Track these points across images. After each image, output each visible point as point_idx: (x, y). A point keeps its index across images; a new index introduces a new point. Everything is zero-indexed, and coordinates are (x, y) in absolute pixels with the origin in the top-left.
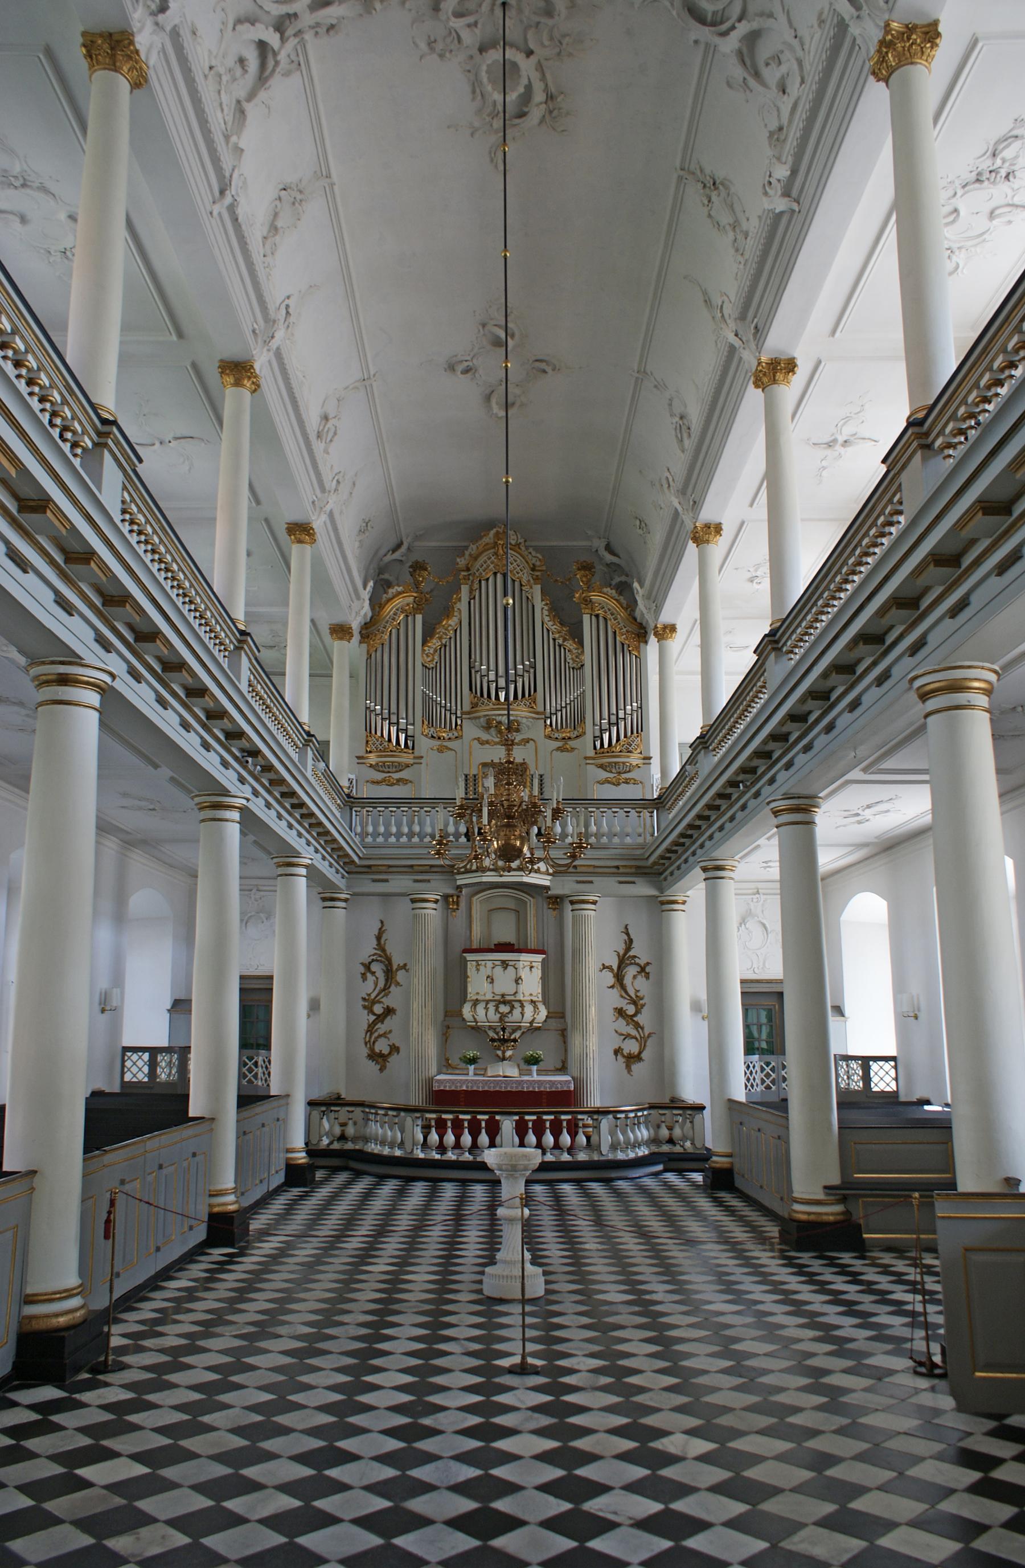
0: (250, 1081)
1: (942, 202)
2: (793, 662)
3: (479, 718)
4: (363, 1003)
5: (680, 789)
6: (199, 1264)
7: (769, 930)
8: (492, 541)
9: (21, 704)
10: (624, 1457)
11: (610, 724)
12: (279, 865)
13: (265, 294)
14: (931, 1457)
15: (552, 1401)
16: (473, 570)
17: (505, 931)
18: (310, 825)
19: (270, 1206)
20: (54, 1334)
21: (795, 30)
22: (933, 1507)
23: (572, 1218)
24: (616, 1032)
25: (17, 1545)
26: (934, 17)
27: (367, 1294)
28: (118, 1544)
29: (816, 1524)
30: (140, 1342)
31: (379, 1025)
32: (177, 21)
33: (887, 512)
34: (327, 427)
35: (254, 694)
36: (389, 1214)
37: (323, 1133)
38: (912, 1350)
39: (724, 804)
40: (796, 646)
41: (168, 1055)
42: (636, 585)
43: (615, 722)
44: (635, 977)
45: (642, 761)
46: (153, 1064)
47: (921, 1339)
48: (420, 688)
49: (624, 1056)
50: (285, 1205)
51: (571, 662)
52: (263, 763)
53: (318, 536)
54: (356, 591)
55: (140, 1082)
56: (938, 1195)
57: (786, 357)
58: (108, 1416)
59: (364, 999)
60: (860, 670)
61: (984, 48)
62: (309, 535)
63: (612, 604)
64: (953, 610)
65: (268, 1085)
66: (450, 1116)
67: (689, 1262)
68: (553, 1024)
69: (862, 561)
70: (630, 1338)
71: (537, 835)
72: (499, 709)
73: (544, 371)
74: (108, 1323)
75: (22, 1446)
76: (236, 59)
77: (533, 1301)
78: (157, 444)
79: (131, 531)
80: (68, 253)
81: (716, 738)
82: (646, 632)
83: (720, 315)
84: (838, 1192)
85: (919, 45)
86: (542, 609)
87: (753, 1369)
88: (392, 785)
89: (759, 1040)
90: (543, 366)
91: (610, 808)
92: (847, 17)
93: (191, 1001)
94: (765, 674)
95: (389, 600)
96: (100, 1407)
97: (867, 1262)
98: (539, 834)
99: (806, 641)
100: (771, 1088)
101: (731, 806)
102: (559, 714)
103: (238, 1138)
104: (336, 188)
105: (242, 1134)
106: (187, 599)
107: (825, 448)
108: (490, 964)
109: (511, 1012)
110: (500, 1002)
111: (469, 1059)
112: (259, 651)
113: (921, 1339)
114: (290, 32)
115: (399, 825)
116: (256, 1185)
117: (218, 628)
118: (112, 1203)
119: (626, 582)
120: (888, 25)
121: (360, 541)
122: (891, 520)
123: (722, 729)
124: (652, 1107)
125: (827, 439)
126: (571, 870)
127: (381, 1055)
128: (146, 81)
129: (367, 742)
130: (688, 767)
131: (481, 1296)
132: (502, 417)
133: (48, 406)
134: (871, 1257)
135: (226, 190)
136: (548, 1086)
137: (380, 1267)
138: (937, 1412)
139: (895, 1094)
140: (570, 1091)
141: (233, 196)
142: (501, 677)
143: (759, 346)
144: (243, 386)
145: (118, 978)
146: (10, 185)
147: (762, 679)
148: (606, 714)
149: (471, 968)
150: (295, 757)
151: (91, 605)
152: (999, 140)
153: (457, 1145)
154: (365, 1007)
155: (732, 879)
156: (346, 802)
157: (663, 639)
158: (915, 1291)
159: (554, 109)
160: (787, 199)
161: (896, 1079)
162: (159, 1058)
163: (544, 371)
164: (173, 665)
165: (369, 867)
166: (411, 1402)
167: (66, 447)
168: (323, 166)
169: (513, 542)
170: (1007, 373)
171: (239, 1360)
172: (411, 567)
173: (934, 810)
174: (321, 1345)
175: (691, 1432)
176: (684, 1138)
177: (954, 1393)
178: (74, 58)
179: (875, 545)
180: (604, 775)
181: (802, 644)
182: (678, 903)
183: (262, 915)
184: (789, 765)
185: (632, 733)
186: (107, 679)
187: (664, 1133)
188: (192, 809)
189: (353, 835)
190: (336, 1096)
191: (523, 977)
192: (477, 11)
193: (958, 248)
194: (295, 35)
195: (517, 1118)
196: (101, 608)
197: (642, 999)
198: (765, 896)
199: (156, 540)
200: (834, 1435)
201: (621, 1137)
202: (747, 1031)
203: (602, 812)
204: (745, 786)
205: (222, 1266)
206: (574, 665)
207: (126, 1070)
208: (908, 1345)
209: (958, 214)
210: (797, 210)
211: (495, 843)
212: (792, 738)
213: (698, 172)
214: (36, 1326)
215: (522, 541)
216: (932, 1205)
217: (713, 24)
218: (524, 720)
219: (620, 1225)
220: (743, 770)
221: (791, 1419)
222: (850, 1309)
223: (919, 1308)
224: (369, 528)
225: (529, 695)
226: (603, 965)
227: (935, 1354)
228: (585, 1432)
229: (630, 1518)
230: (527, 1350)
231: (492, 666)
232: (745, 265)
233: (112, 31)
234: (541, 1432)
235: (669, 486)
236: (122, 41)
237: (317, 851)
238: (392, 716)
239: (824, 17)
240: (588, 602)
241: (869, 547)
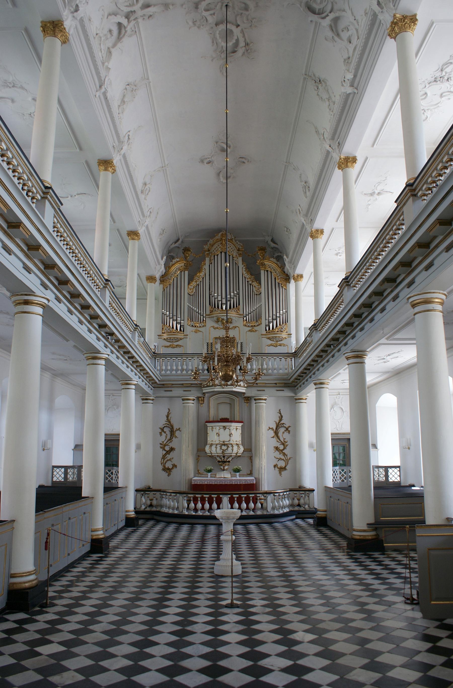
0: (109, 481)
1: (420, 90)
2: (355, 291)
3: (214, 317)
4: (160, 446)
5: (305, 348)
6: (87, 561)
7: (344, 411)
8: (220, 238)
9: (8, 313)
10: (276, 642)
11: (273, 319)
12: (123, 384)
13: (119, 130)
14: (411, 638)
15: (245, 619)
16: (211, 251)
17: (225, 413)
18: (137, 366)
19: (118, 536)
20: (24, 591)
21: (355, 17)
22: (411, 659)
23: (254, 540)
24: (275, 457)
25: (11, 679)
26: (415, 13)
27: (162, 574)
28: (55, 679)
29: (360, 668)
30: (61, 595)
31: (167, 455)
32: (82, 15)
33: (397, 224)
34: (146, 187)
35: (112, 308)
36: (172, 539)
37: (142, 503)
38: (404, 593)
39: (324, 355)
40: (357, 284)
41: (73, 469)
42: (285, 257)
43: (275, 318)
44: (283, 433)
45: (288, 336)
46: (66, 473)
47: (409, 588)
48: (187, 304)
49: (278, 468)
50: (125, 535)
51: (255, 291)
52: (115, 338)
53: (141, 237)
54: (158, 261)
55: (60, 481)
56: (417, 526)
57: (352, 156)
58: (48, 626)
59: (161, 444)
60: (385, 294)
61: (436, 26)
62: (137, 236)
63: (274, 265)
64: (427, 267)
65: (118, 483)
66: (200, 496)
67: (307, 558)
68: (246, 454)
69: (386, 246)
70: (280, 591)
71: (239, 370)
72: (223, 313)
73: (244, 162)
74: (47, 586)
75: (11, 638)
76: (108, 30)
77: (236, 576)
78: (70, 197)
79: (57, 236)
80: (32, 115)
81: (321, 325)
82: (289, 278)
83: (323, 138)
84: (373, 526)
85: (409, 24)
86: (243, 268)
87: (334, 603)
88: (174, 348)
89: (339, 460)
90: (243, 160)
91: (273, 357)
92: (377, 12)
93: (83, 445)
94: (343, 296)
95: (173, 265)
96: (44, 622)
97: (385, 556)
98: (241, 369)
99: (361, 281)
100: (344, 481)
101: (327, 355)
102: (250, 315)
103: (104, 506)
104: (151, 84)
105: (106, 504)
106: (82, 266)
107: (370, 196)
108: (218, 428)
109: (227, 449)
110: (222, 445)
111: (208, 470)
112: (114, 288)
113: (409, 588)
114: (132, 18)
115: (177, 366)
116: (112, 526)
117: (96, 278)
118: (48, 534)
119: (280, 256)
120: (395, 15)
121: (160, 239)
122: (399, 227)
123: (323, 321)
124: (291, 490)
125: (370, 192)
126: (255, 385)
127: (168, 469)
128: (68, 40)
129: (163, 328)
130: (308, 338)
131: (213, 574)
132: (224, 183)
133: (21, 181)
134: (387, 554)
135: (102, 86)
136: (244, 481)
137: (168, 562)
138: (414, 619)
139: (399, 483)
140: (254, 484)
141: (105, 88)
142: (224, 298)
143: (340, 151)
144: (108, 170)
145: (50, 435)
146: (8, 86)
147: (342, 299)
148: (271, 315)
149: (209, 429)
150: (130, 336)
151: (39, 269)
152: (444, 64)
153: (203, 508)
154: (161, 448)
155: (327, 388)
156: (153, 355)
157: (297, 281)
158: (406, 568)
159: (249, 49)
160: (352, 88)
161: (400, 476)
162: (69, 471)
163: (244, 162)
164: (75, 295)
165: (163, 384)
166: (182, 620)
167: (29, 199)
168: (145, 75)
169: (229, 238)
170: (449, 163)
171: (105, 602)
172: (183, 250)
173: (418, 356)
174: (142, 596)
175: (306, 631)
176: (305, 504)
177: (422, 611)
178: (37, 32)
179: (392, 239)
180: (270, 342)
181: (359, 283)
182: (303, 399)
183: (115, 407)
184: (353, 337)
185: (283, 323)
186: (46, 302)
187: (296, 502)
188: (84, 360)
189: (156, 370)
190: (148, 487)
191: (233, 433)
192: (215, 9)
193: (427, 109)
194: (134, 20)
195: (230, 496)
196: (44, 270)
197: (286, 442)
198: (342, 396)
199: (68, 239)
200: (369, 630)
201: (277, 504)
202: (334, 456)
203: (269, 359)
204: (334, 347)
205: (97, 562)
206: (257, 293)
207: (54, 476)
208: (402, 591)
209: (427, 95)
210: (357, 92)
211: (221, 373)
212: (355, 325)
213: (313, 76)
214: (16, 587)
215: (234, 237)
216: (414, 530)
217: (319, 14)
218: (234, 318)
219: (276, 542)
220: (333, 339)
221: (351, 624)
222: (378, 576)
223: (408, 575)
224: (164, 233)
225: (236, 306)
226: (269, 427)
227: (414, 595)
228: (260, 632)
229: (279, 668)
230: (234, 597)
231: (220, 294)
232: (333, 116)
233: (54, 20)
234: (239, 632)
235: (300, 213)
236: (58, 24)
237: (140, 378)
238: (174, 317)
239: (367, 11)
240: (263, 264)
241: (389, 240)
